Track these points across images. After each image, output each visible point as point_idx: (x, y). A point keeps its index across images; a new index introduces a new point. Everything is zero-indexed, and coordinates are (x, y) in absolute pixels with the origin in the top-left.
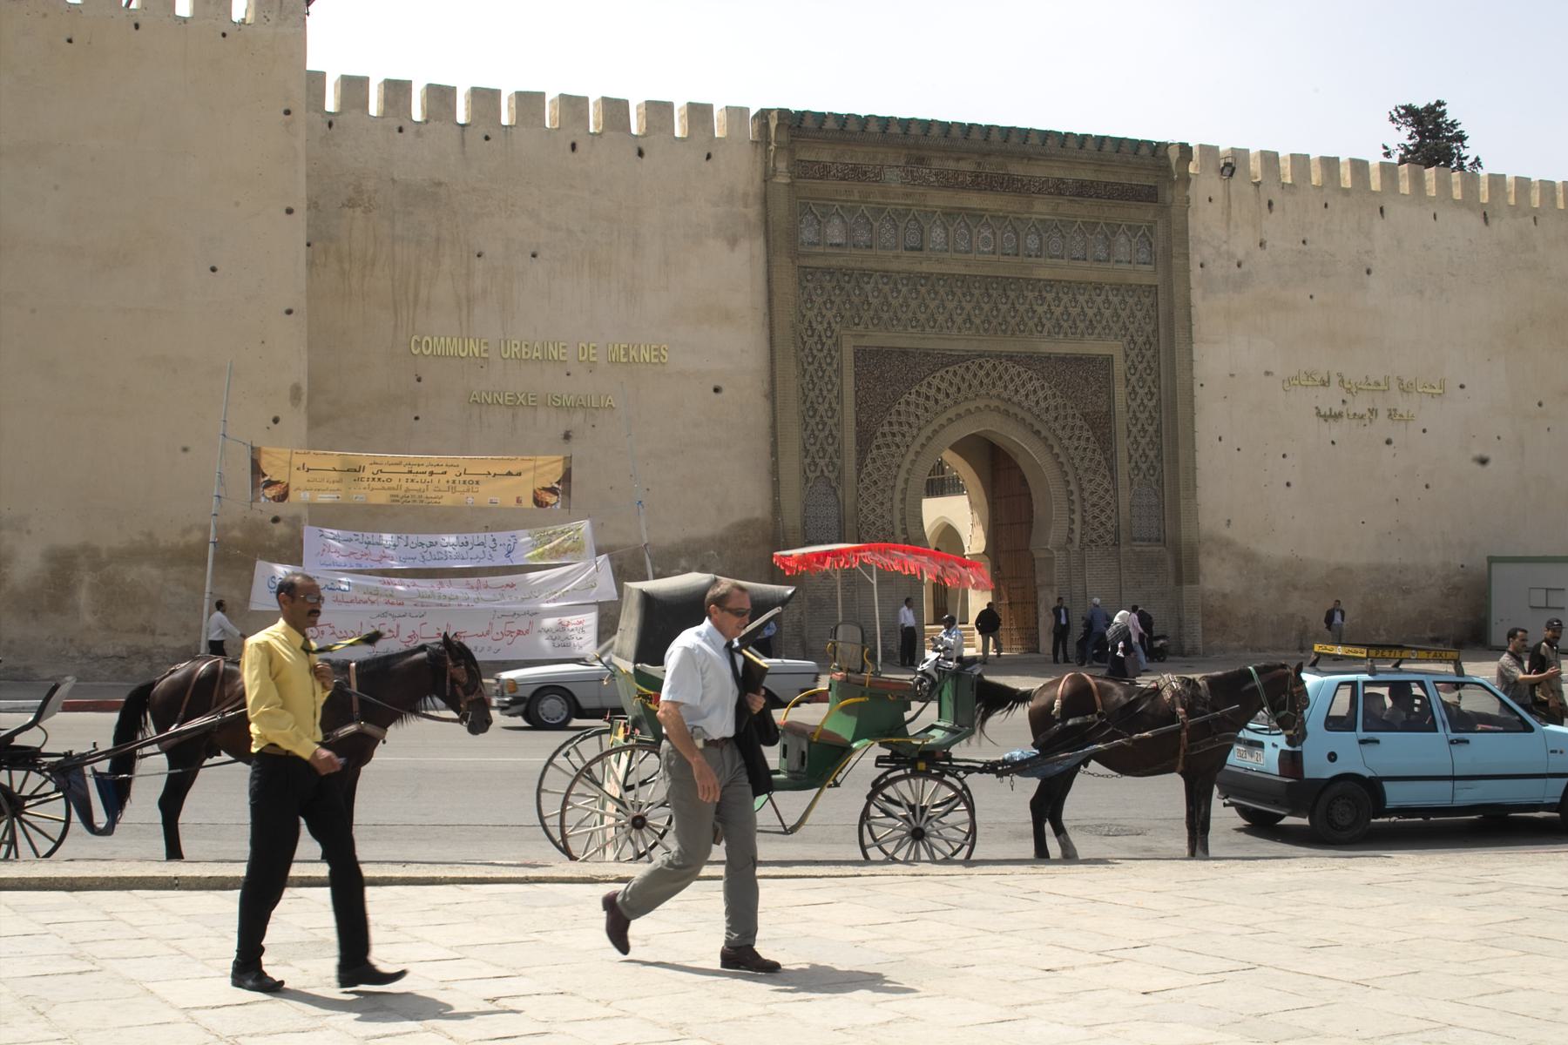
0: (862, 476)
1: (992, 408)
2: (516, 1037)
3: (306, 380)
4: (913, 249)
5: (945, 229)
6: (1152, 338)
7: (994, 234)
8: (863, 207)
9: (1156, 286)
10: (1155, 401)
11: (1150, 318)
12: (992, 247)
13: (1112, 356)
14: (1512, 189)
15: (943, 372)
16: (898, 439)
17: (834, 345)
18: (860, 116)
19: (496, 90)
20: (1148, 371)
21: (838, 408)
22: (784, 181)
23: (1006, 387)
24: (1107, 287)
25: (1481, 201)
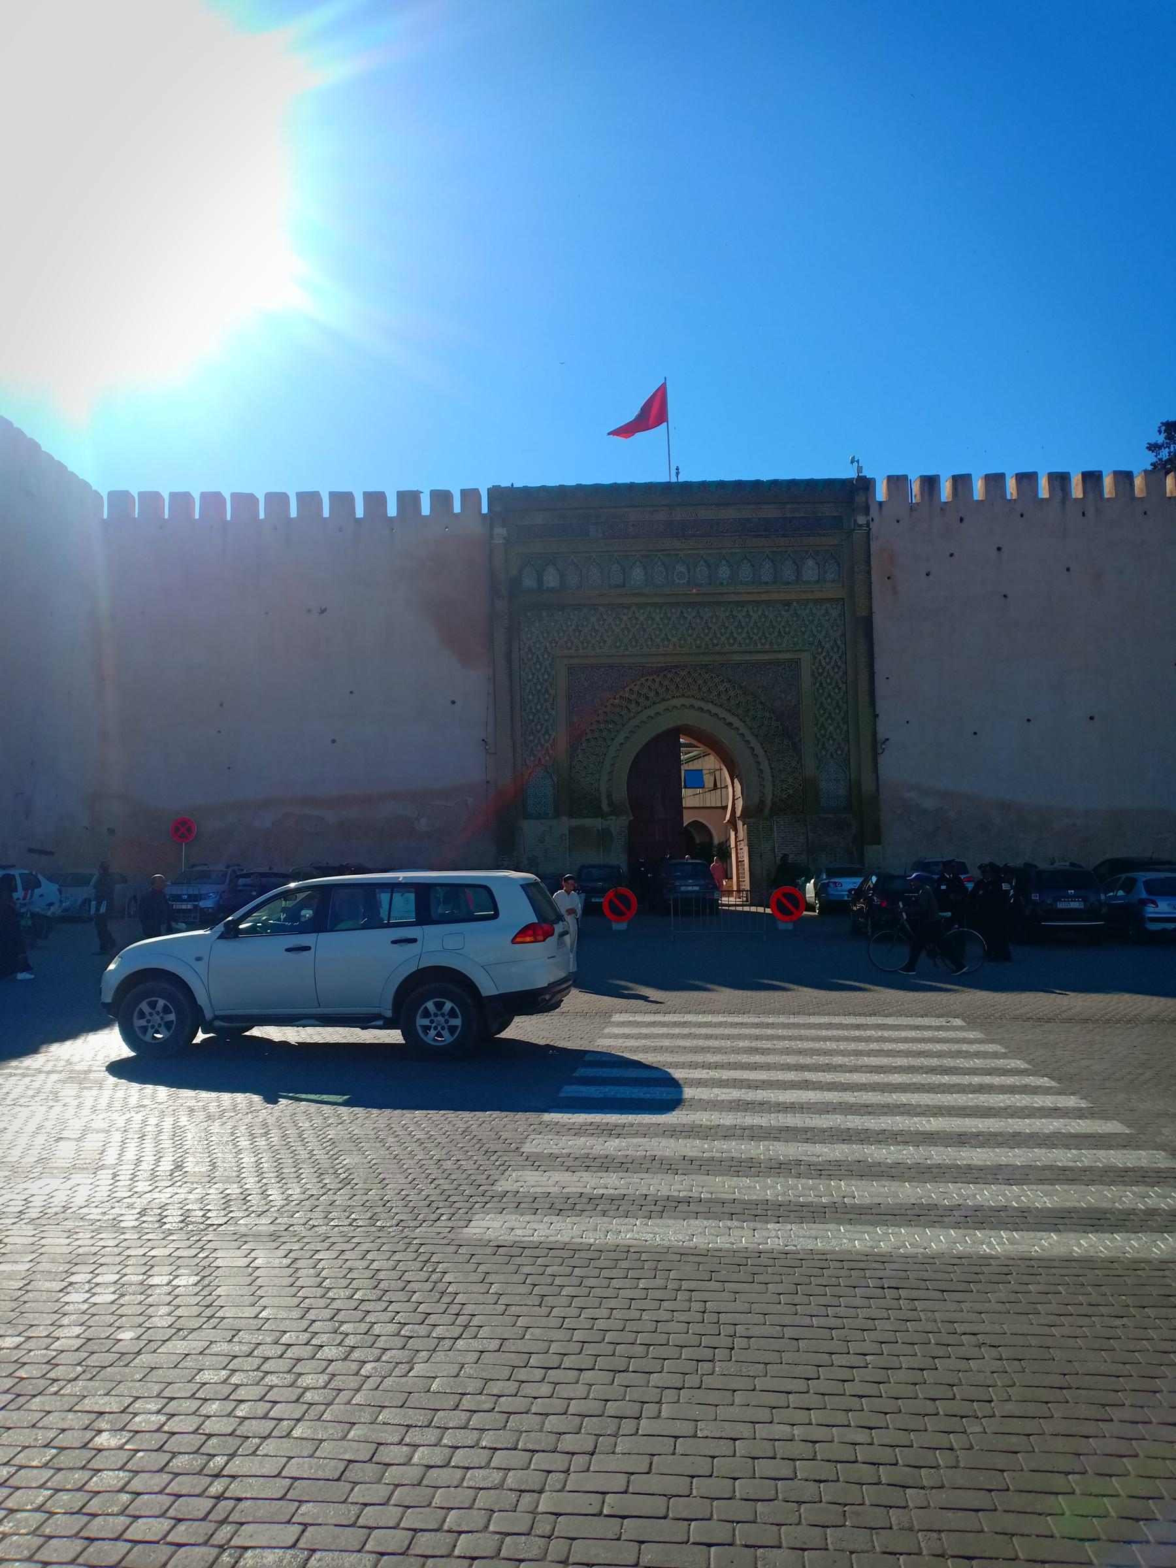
0: (574, 763)
1: (679, 707)
2: (653, 1494)
3: (504, 1037)
4: (617, 586)
5: (645, 568)
6: (839, 643)
7: (688, 568)
8: (573, 557)
9: (843, 599)
10: (842, 694)
11: (837, 626)
12: (686, 579)
13: (800, 659)
14: (916, 488)
15: (643, 680)
16: (604, 734)
17: (550, 665)
18: (91, 487)
19: (1062, 474)
20: (836, 670)
21: (554, 713)
22: (501, 542)
23: (700, 689)
24: (795, 604)
25: (1040, 497)
